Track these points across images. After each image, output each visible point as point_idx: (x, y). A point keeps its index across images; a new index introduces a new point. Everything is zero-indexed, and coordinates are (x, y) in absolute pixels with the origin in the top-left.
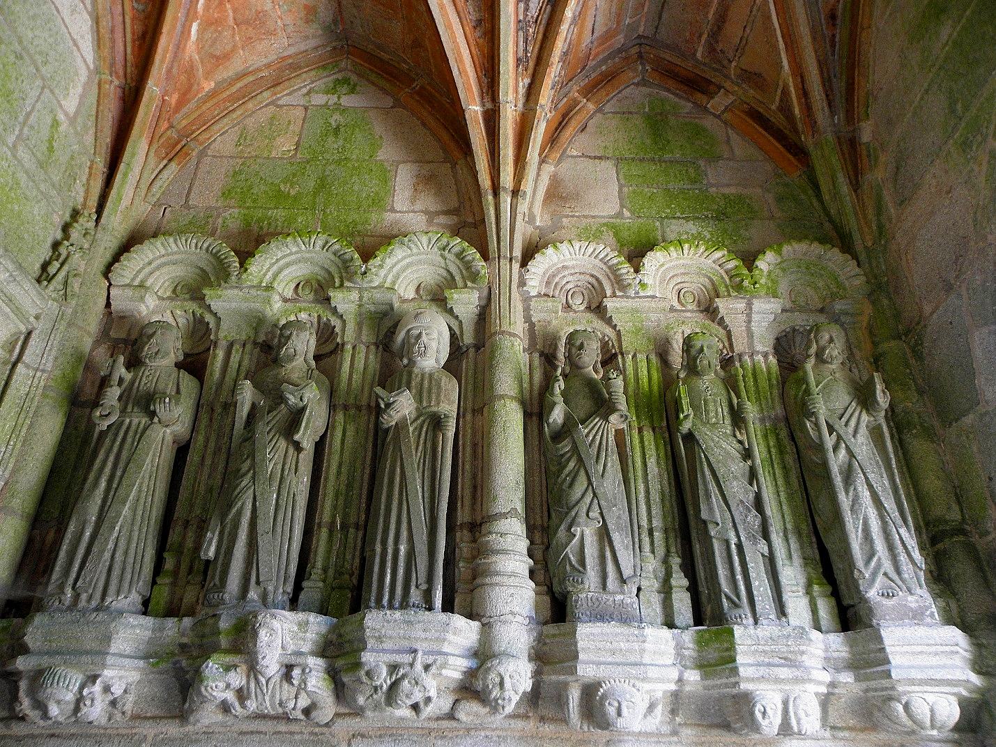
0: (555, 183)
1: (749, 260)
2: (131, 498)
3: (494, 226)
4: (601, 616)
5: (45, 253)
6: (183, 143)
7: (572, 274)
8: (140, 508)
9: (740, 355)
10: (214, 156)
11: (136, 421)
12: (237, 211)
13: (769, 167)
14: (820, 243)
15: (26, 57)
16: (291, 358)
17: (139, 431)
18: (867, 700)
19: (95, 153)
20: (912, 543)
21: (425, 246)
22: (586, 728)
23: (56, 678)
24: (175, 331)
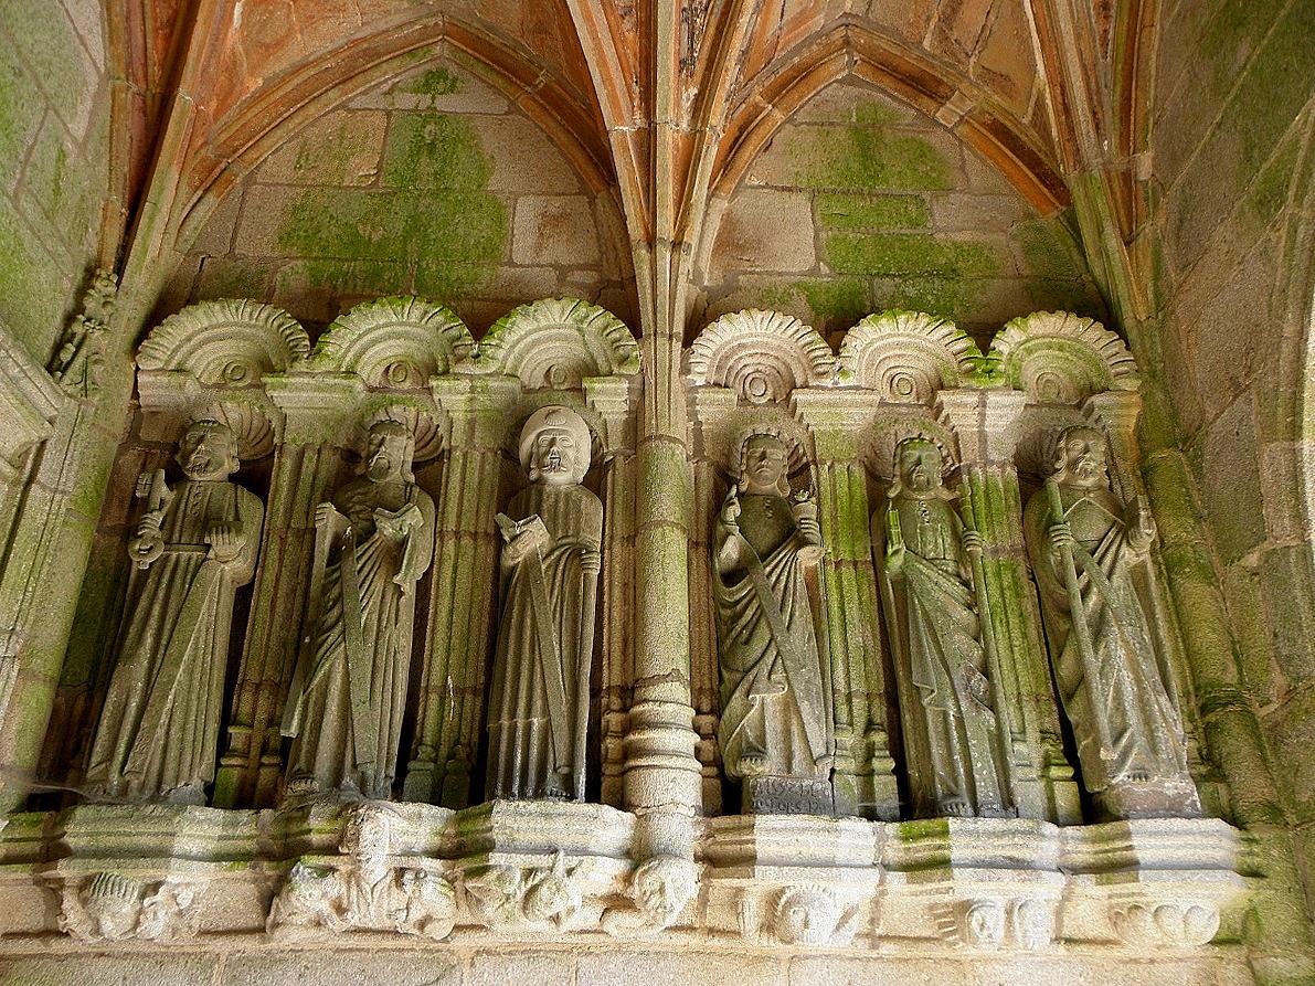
0: (729, 223)
2: (185, 658)
6: (223, 166)
7: (751, 355)
10: (265, 184)
11: (185, 555)
12: (300, 263)
14: (868, 820)
15: (26, 72)
17: (191, 569)
18: (1111, 907)
19: (110, 189)
23: (110, 886)
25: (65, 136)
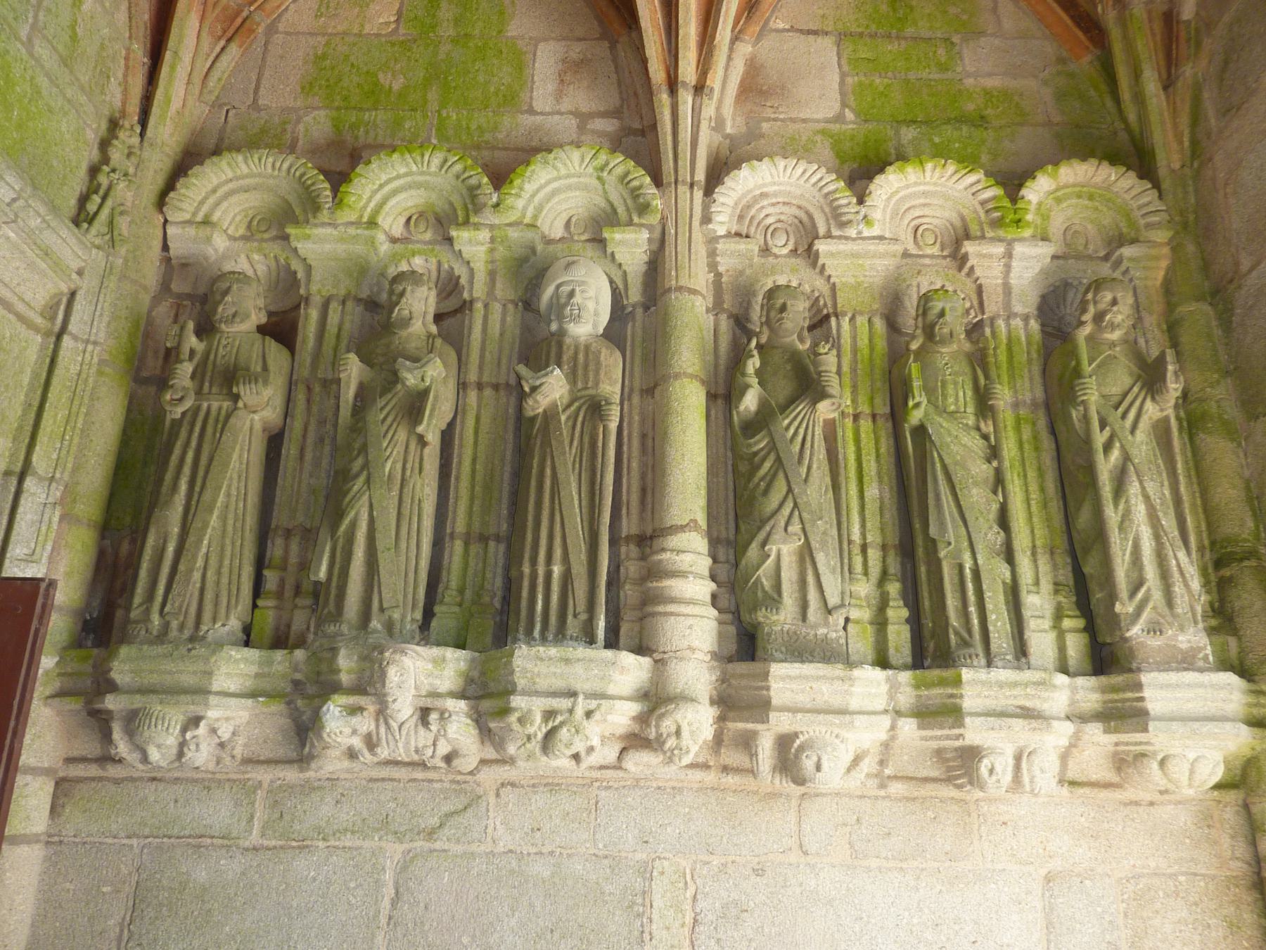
0: (753, 68)
1: (1012, 182)
2: (219, 504)
3: (669, 138)
4: (801, 651)
5: (78, 182)
6: (245, 14)
7: (773, 205)
8: (231, 516)
9: (992, 320)
10: (287, 33)
11: (215, 405)
12: (322, 113)
13: (1050, 48)
16: (406, 322)
17: (221, 419)
19: (130, 37)
20: (1192, 571)
21: (576, 165)
22: (777, 781)
24: (255, 285)
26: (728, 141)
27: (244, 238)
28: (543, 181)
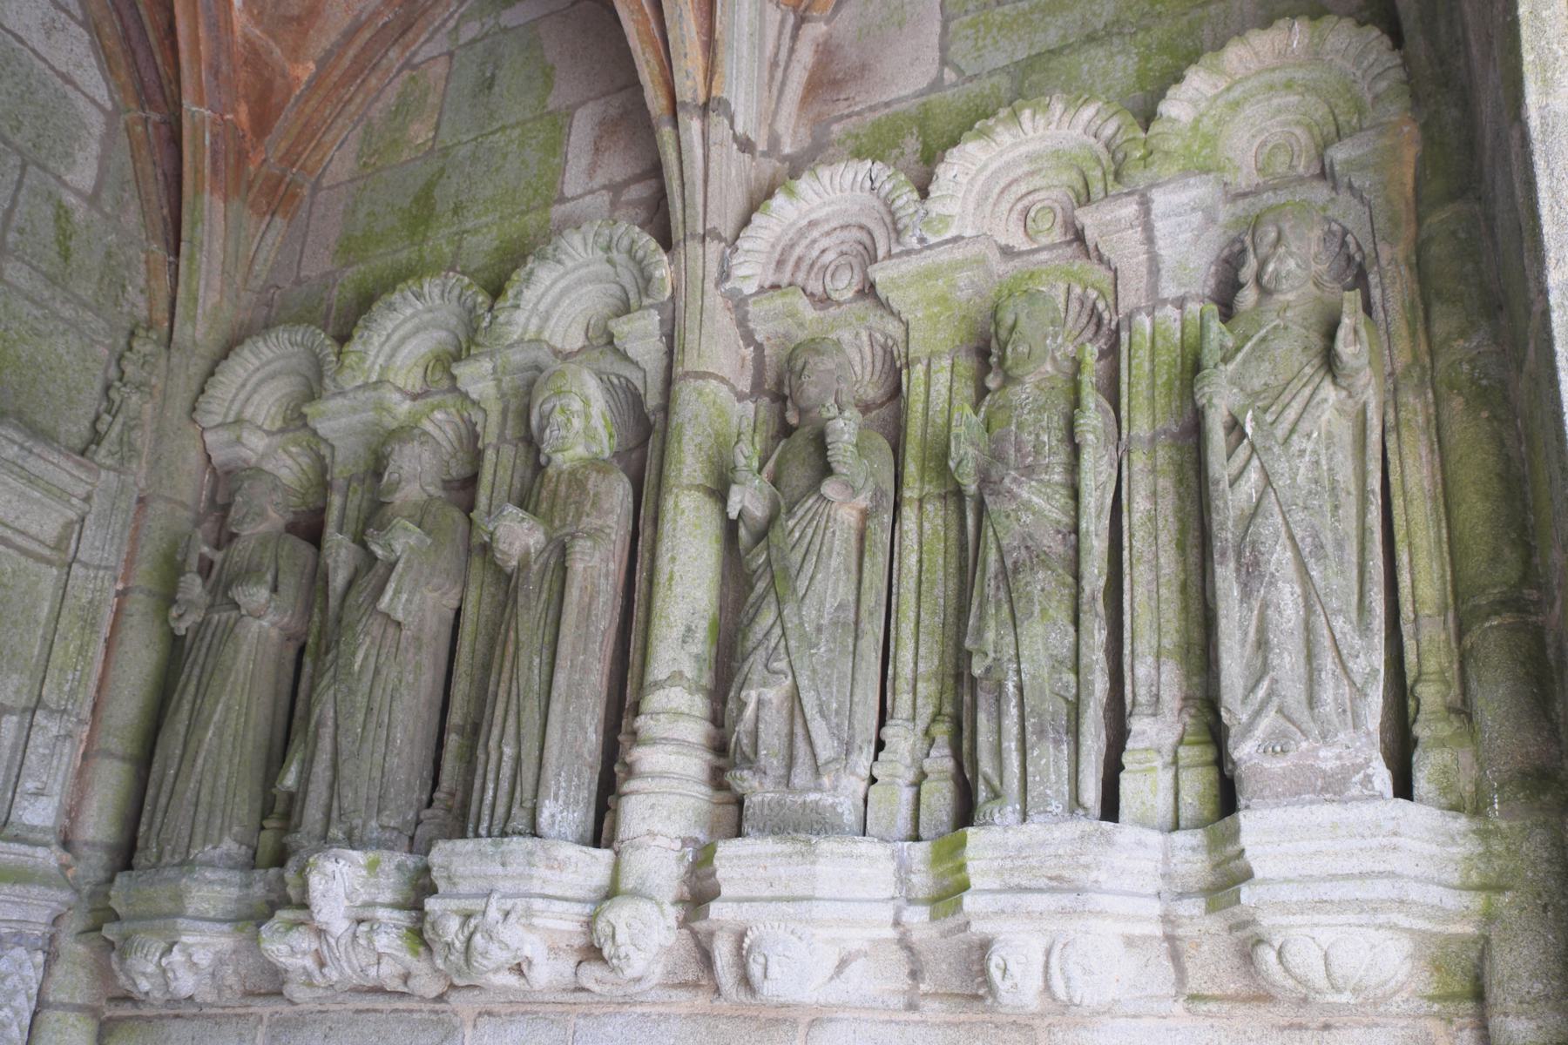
7: (828, 234)
21: (581, 249)
25: (62, 190)
26: (787, 164)
27: (282, 431)
28: (548, 283)
